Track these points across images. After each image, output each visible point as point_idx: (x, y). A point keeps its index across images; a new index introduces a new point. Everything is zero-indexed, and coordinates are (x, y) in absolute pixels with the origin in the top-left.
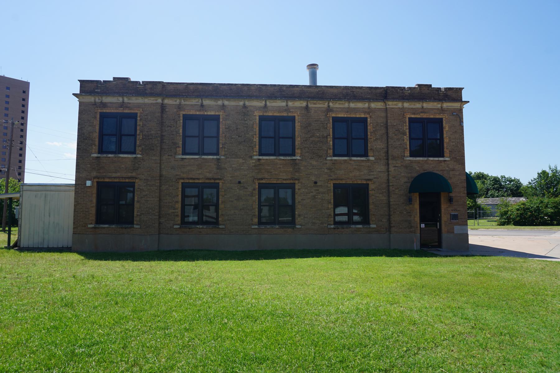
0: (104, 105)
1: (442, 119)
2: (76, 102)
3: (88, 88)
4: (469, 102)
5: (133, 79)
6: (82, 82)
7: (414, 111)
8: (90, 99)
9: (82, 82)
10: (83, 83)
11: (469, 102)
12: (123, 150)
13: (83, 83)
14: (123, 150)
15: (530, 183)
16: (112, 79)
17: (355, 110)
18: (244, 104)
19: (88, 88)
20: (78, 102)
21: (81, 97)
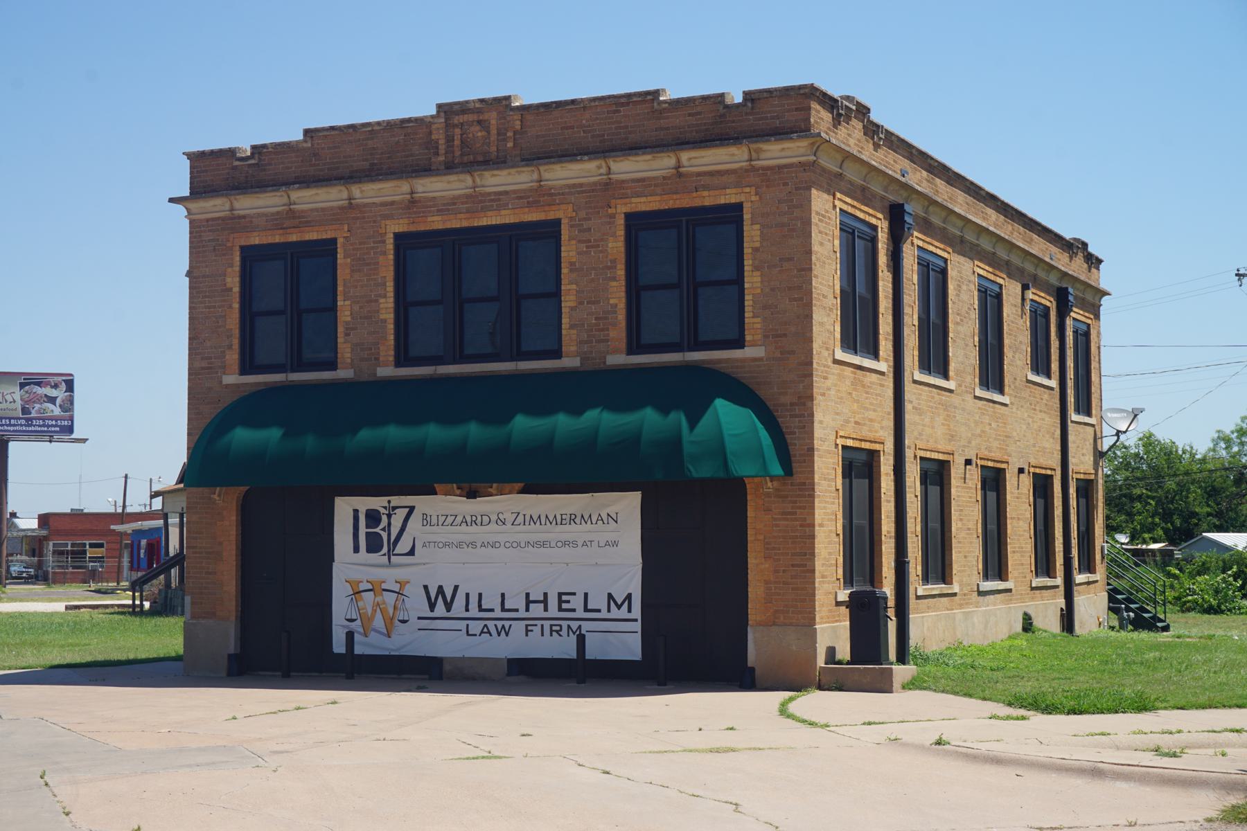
0: (413, 203)
1: (557, 223)
2: (178, 224)
3: (214, 174)
4: (171, 200)
5: (525, 96)
6: (190, 156)
7: (644, 185)
8: (216, 206)
9: (190, 156)
10: (200, 161)
11: (171, 200)
12: (703, 337)
13: (200, 161)
14: (703, 337)
15: (13, 515)
16: (434, 112)
17: (499, 200)
18: (678, 166)
19: (214, 174)
20: (187, 221)
21: (193, 206)
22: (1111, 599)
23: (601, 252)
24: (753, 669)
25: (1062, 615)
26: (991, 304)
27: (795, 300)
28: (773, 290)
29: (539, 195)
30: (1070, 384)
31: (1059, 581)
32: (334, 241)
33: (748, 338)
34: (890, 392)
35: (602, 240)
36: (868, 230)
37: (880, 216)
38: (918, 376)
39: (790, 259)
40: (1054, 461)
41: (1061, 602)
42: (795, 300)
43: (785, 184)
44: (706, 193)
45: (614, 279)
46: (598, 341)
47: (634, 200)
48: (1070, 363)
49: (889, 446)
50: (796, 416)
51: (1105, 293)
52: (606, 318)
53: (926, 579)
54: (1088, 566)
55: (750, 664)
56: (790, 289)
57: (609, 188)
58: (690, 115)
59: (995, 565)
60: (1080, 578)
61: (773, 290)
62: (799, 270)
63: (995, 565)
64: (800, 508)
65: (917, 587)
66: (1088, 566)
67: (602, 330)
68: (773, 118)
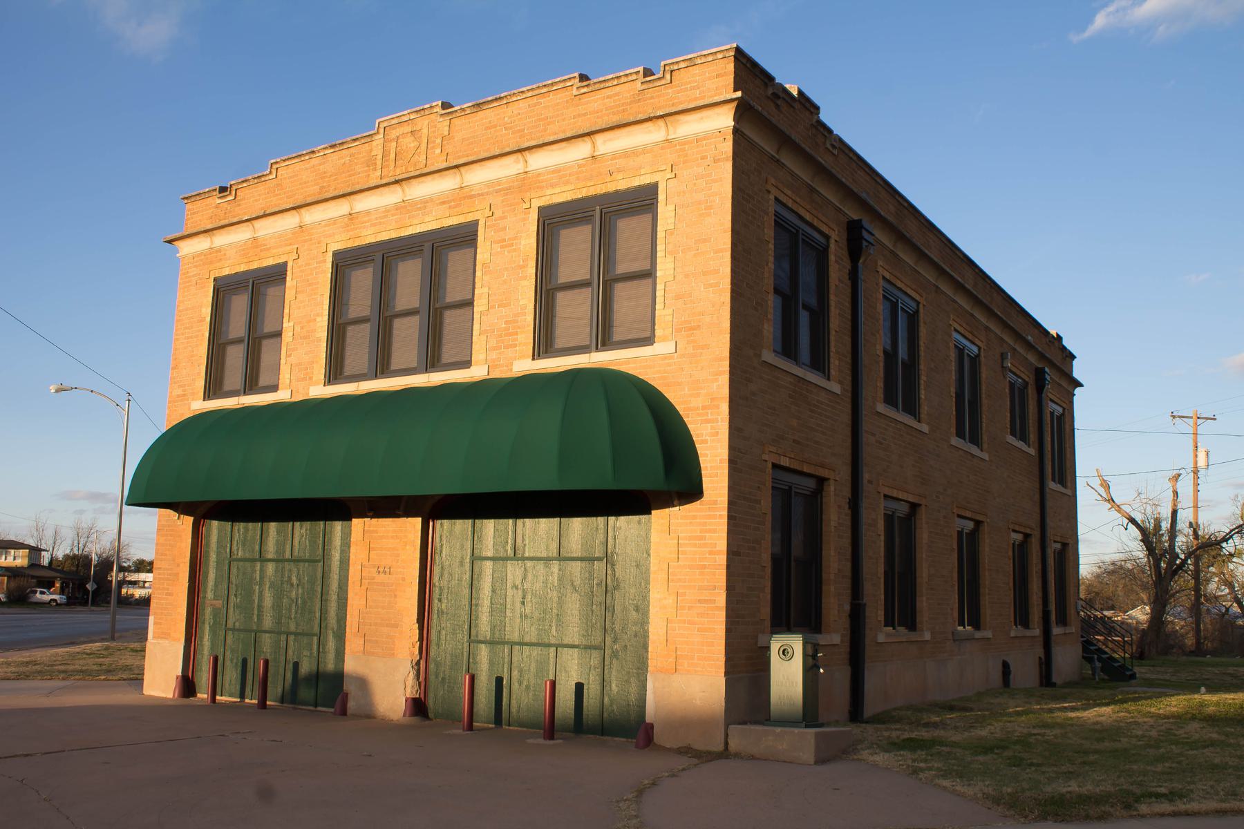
22: (1085, 649)
23: (515, 250)
24: (651, 726)
25: (1040, 664)
26: (969, 368)
27: (711, 285)
28: (687, 276)
29: (463, 196)
30: (1048, 456)
31: (1037, 632)
32: (285, 264)
33: (658, 332)
34: (846, 418)
35: (515, 238)
36: (822, 240)
37: (833, 226)
38: (881, 408)
39: (705, 241)
40: (1034, 521)
41: (1040, 652)
42: (711, 285)
43: (703, 158)
44: (620, 176)
45: (525, 278)
46: (507, 347)
47: (549, 192)
48: (1048, 439)
49: (844, 473)
50: (708, 421)
51: (1080, 385)
52: (515, 321)
53: (889, 622)
54: (1063, 621)
55: (648, 720)
56: (705, 273)
57: (526, 182)
58: (608, 97)
59: (972, 613)
60: (1056, 630)
61: (687, 276)
62: (716, 252)
63: (972, 613)
64: (710, 531)
65: (880, 634)
66: (1063, 621)
67: (510, 334)
68: (693, 88)
